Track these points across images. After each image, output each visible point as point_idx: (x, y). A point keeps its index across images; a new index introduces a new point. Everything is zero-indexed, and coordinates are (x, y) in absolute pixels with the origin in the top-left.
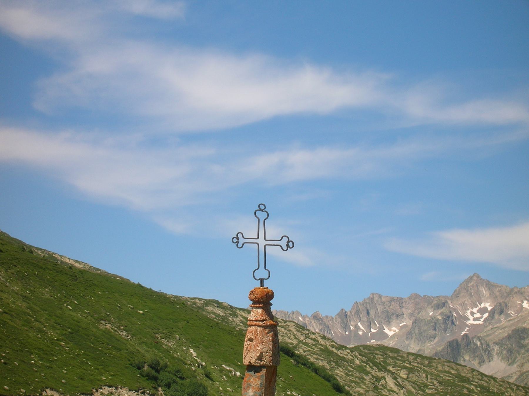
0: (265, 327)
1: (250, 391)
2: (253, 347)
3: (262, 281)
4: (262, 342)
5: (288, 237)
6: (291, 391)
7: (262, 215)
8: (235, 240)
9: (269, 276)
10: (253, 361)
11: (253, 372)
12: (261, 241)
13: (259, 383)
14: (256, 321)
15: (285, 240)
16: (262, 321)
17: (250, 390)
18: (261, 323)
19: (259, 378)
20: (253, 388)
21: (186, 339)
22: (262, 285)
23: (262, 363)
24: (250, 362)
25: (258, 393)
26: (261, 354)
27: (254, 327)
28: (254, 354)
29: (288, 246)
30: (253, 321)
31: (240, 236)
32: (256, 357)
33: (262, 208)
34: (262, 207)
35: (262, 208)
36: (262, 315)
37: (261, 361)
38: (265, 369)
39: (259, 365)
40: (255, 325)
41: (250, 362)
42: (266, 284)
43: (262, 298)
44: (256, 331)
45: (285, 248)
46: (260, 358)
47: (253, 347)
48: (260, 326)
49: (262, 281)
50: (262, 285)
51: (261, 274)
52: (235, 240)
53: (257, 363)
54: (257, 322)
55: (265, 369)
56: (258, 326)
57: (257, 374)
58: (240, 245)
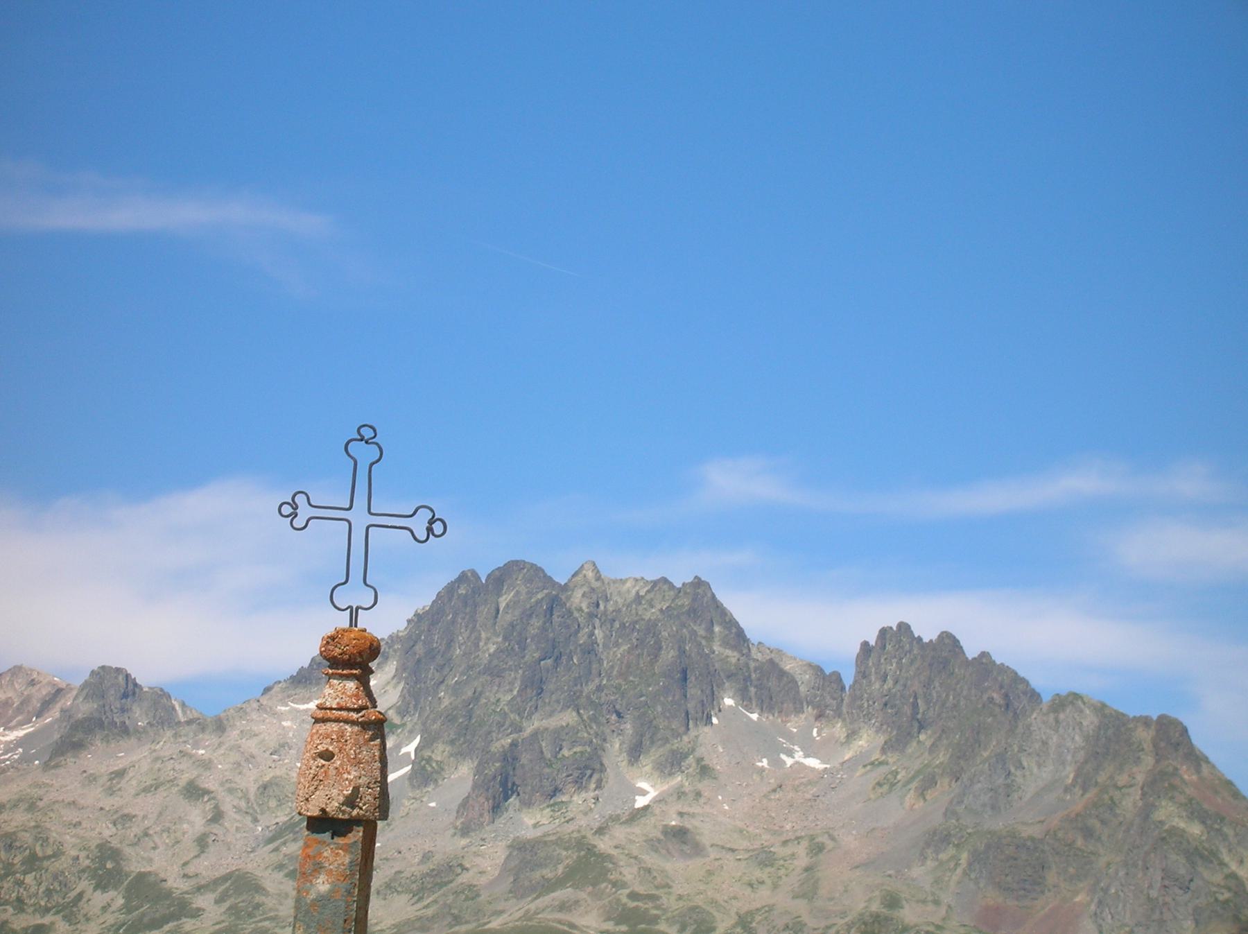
0: (365, 726)
1: (320, 881)
2: (332, 772)
3: (354, 613)
4: (357, 762)
5: (432, 510)
6: (799, 756)
7: (366, 454)
8: (287, 510)
9: (375, 603)
10: (332, 808)
11: (327, 835)
12: (360, 518)
13: (347, 860)
14: (349, 710)
15: (425, 515)
16: (358, 710)
17: (322, 878)
18: (354, 716)
19: (346, 848)
20: (330, 872)
21: (1033, 710)
22: (353, 620)
23: (355, 812)
24: (323, 810)
25: (343, 886)
26: (356, 789)
27: (334, 725)
28: (335, 792)
29: (430, 530)
30: (331, 709)
31: (301, 500)
32: (342, 799)
33: (366, 435)
34: (367, 433)
35: (366, 435)
36: (357, 696)
37: (353, 808)
38: (361, 829)
39: (346, 817)
40: (337, 720)
41: (323, 810)
42: (364, 620)
43: (360, 653)
44: (341, 734)
45: (422, 535)
46: (351, 801)
47: (332, 772)
48: (353, 723)
49: (354, 613)
50: (353, 620)
51: (355, 595)
52: (287, 510)
53: (344, 812)
54: (344, 713)
55: (361, 829)
56: (346, 721)
57: (340, 841)
58: (299, 522)
